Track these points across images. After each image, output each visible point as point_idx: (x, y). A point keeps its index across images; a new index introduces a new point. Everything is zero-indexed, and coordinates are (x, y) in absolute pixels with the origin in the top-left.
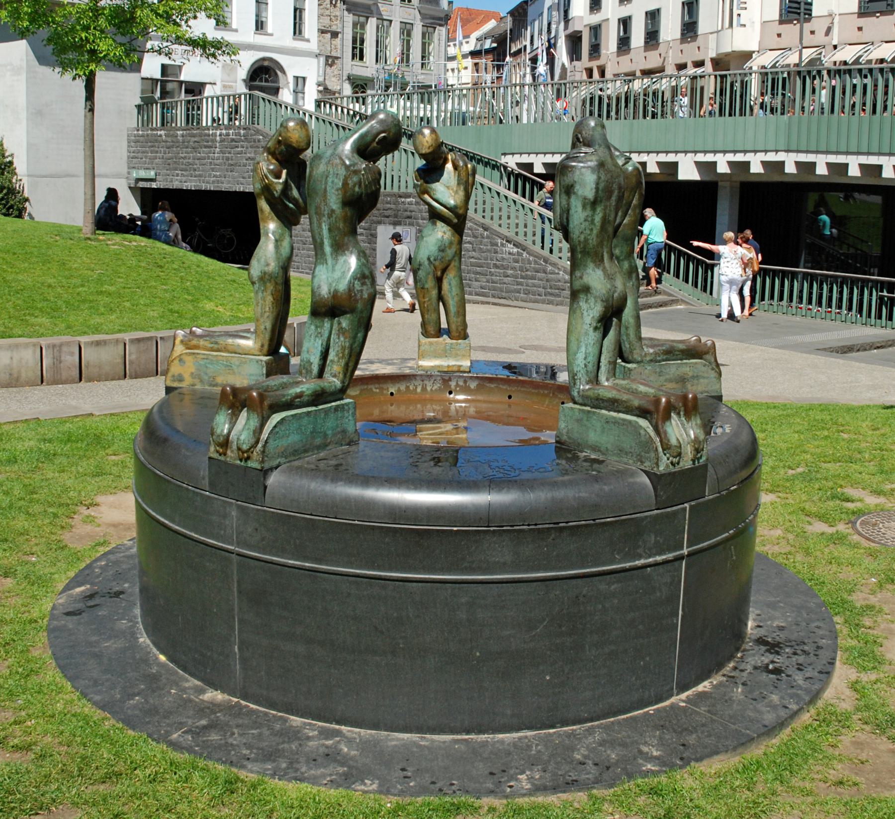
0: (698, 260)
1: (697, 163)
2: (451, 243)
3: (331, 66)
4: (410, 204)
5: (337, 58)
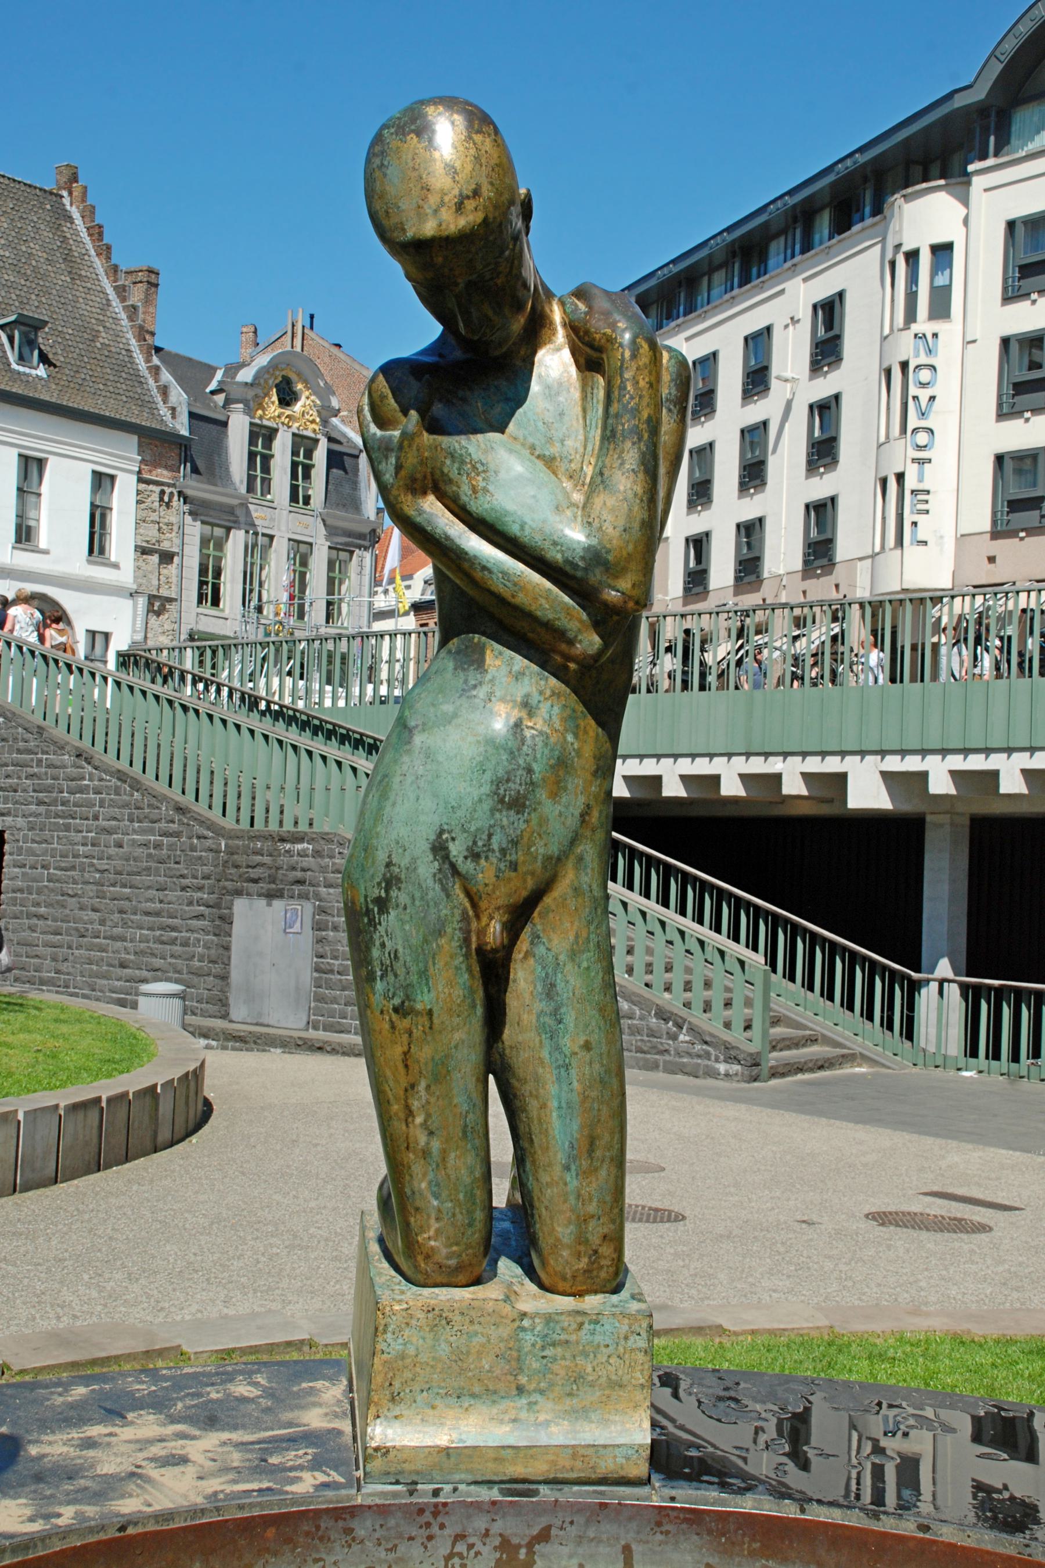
0: (893, 972)
1: (884, 774)
2: (562, 764)
3: (158, 614)
4: (302, 854)
5: (170, 600)
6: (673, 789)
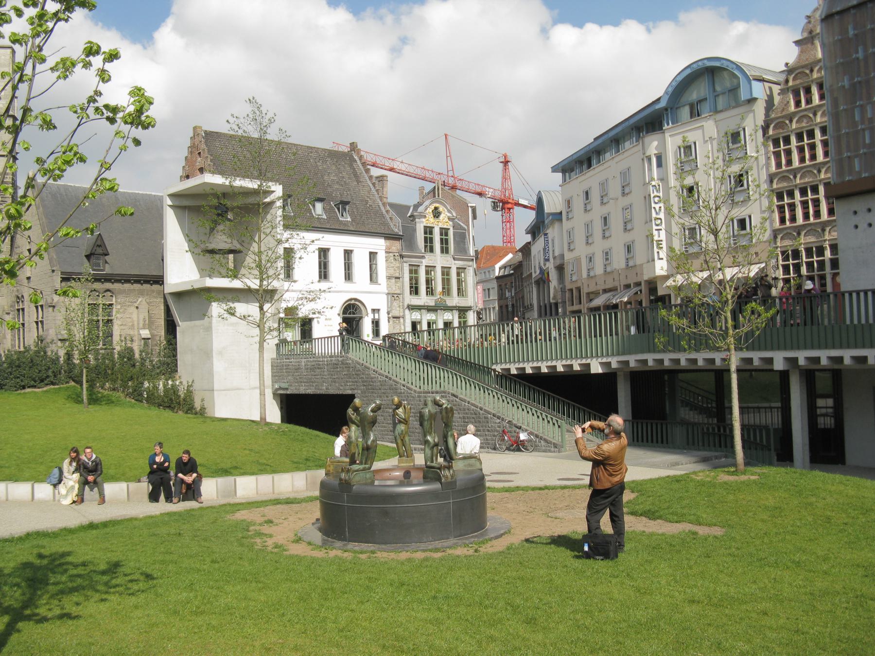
6: (545, 370)
